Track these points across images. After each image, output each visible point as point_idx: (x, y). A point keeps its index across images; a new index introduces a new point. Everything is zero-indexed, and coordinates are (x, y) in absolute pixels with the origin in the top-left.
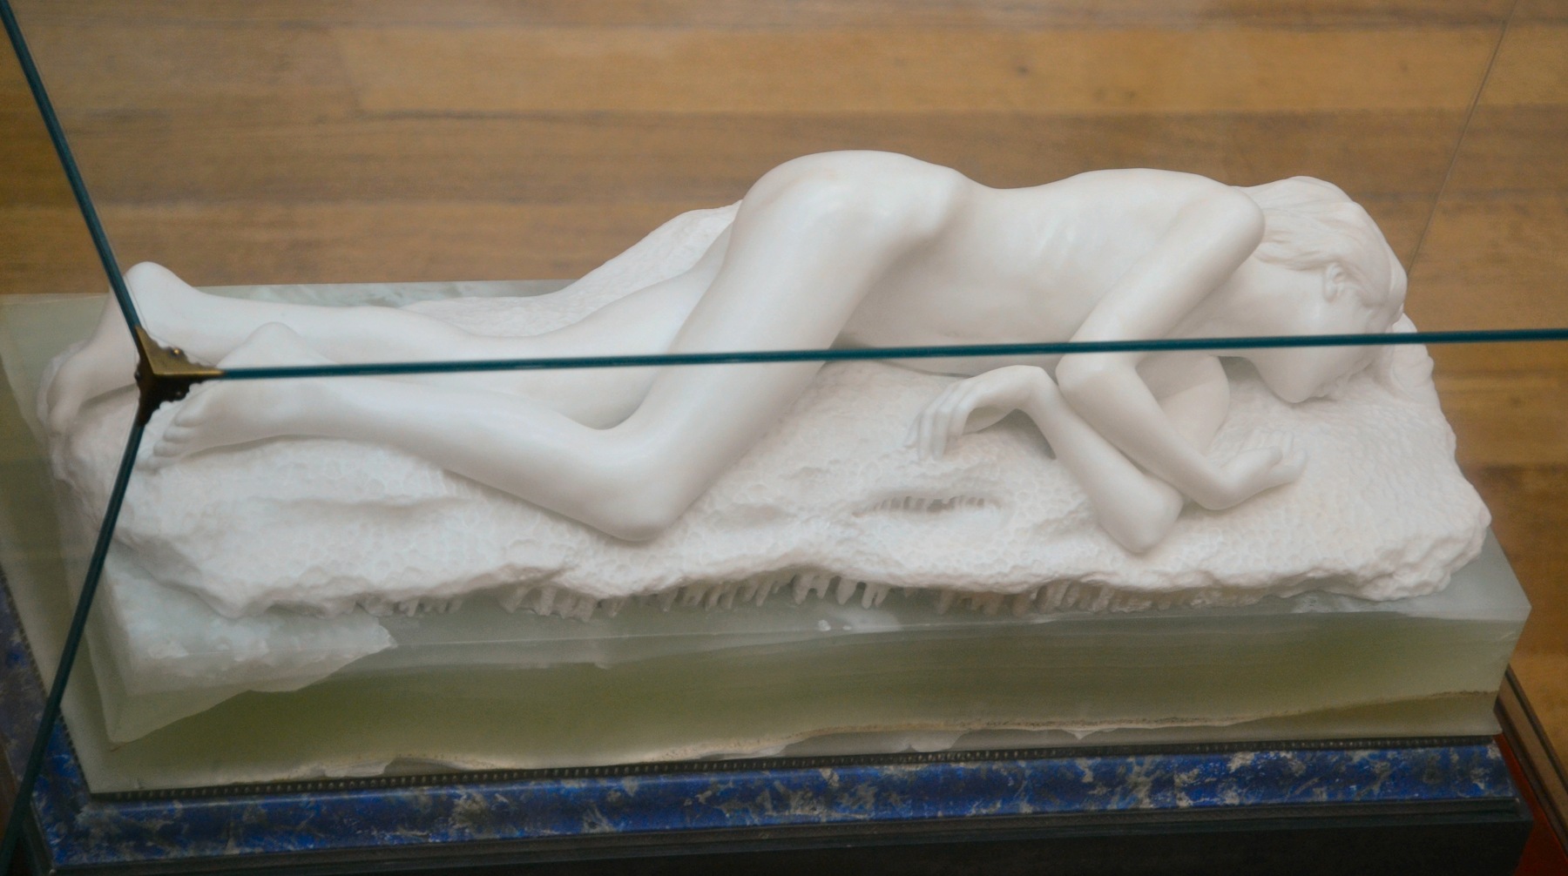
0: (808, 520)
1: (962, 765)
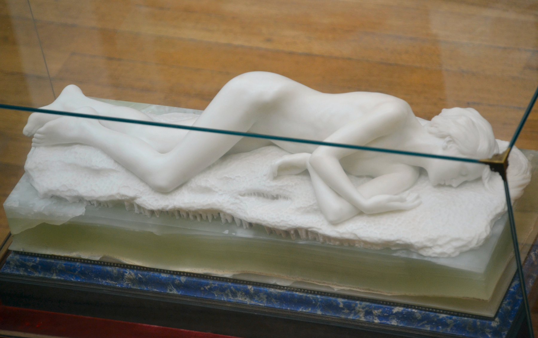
0: (222, 194)
1: (297, 293)
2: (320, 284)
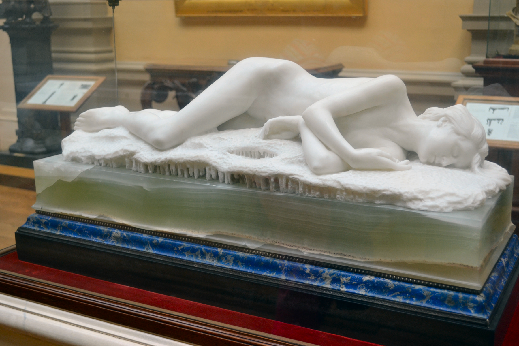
0: (212, 150)
2: (290, 248)
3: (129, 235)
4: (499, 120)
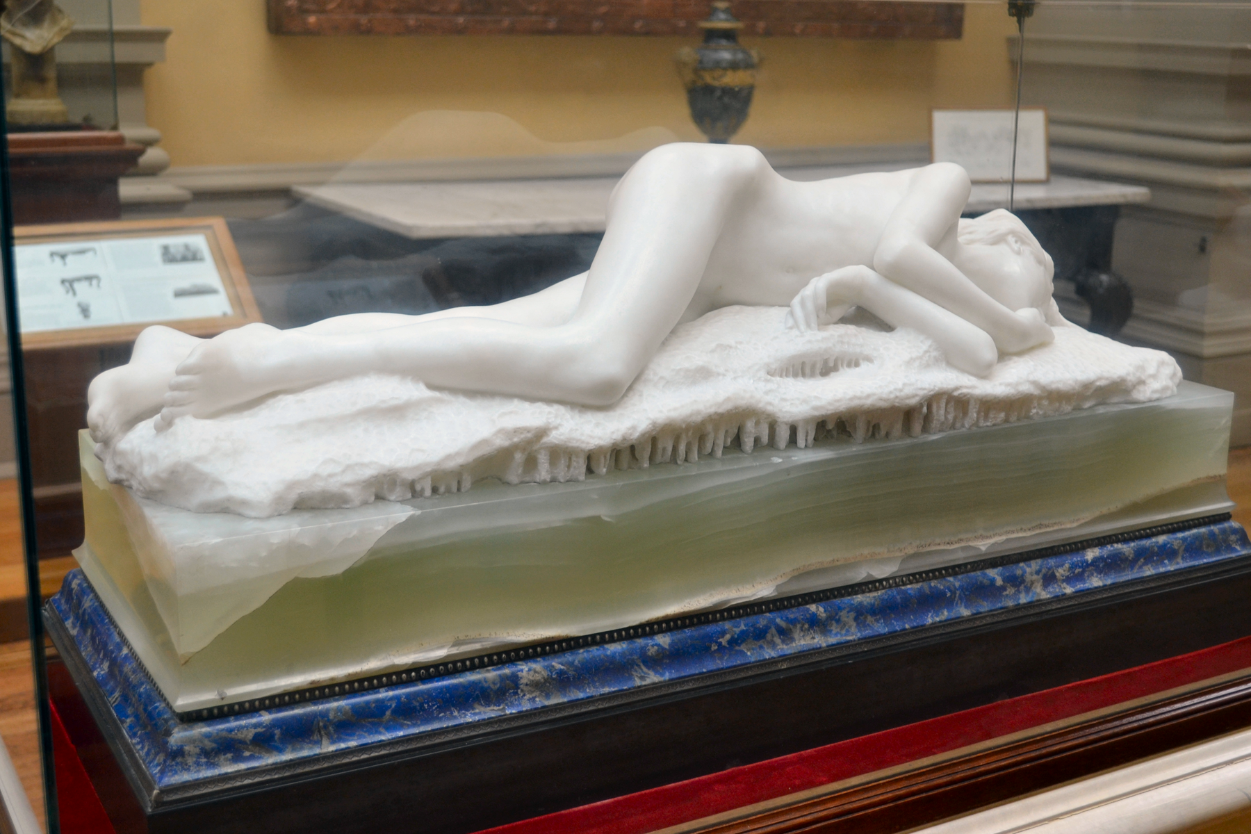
3: (571, 664)
4: (89, 278)
